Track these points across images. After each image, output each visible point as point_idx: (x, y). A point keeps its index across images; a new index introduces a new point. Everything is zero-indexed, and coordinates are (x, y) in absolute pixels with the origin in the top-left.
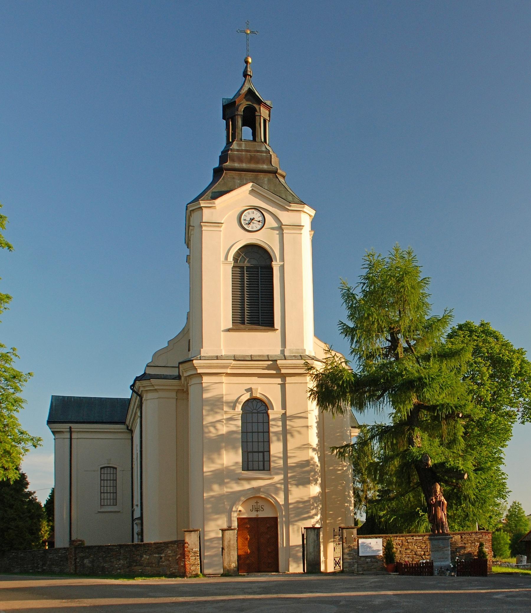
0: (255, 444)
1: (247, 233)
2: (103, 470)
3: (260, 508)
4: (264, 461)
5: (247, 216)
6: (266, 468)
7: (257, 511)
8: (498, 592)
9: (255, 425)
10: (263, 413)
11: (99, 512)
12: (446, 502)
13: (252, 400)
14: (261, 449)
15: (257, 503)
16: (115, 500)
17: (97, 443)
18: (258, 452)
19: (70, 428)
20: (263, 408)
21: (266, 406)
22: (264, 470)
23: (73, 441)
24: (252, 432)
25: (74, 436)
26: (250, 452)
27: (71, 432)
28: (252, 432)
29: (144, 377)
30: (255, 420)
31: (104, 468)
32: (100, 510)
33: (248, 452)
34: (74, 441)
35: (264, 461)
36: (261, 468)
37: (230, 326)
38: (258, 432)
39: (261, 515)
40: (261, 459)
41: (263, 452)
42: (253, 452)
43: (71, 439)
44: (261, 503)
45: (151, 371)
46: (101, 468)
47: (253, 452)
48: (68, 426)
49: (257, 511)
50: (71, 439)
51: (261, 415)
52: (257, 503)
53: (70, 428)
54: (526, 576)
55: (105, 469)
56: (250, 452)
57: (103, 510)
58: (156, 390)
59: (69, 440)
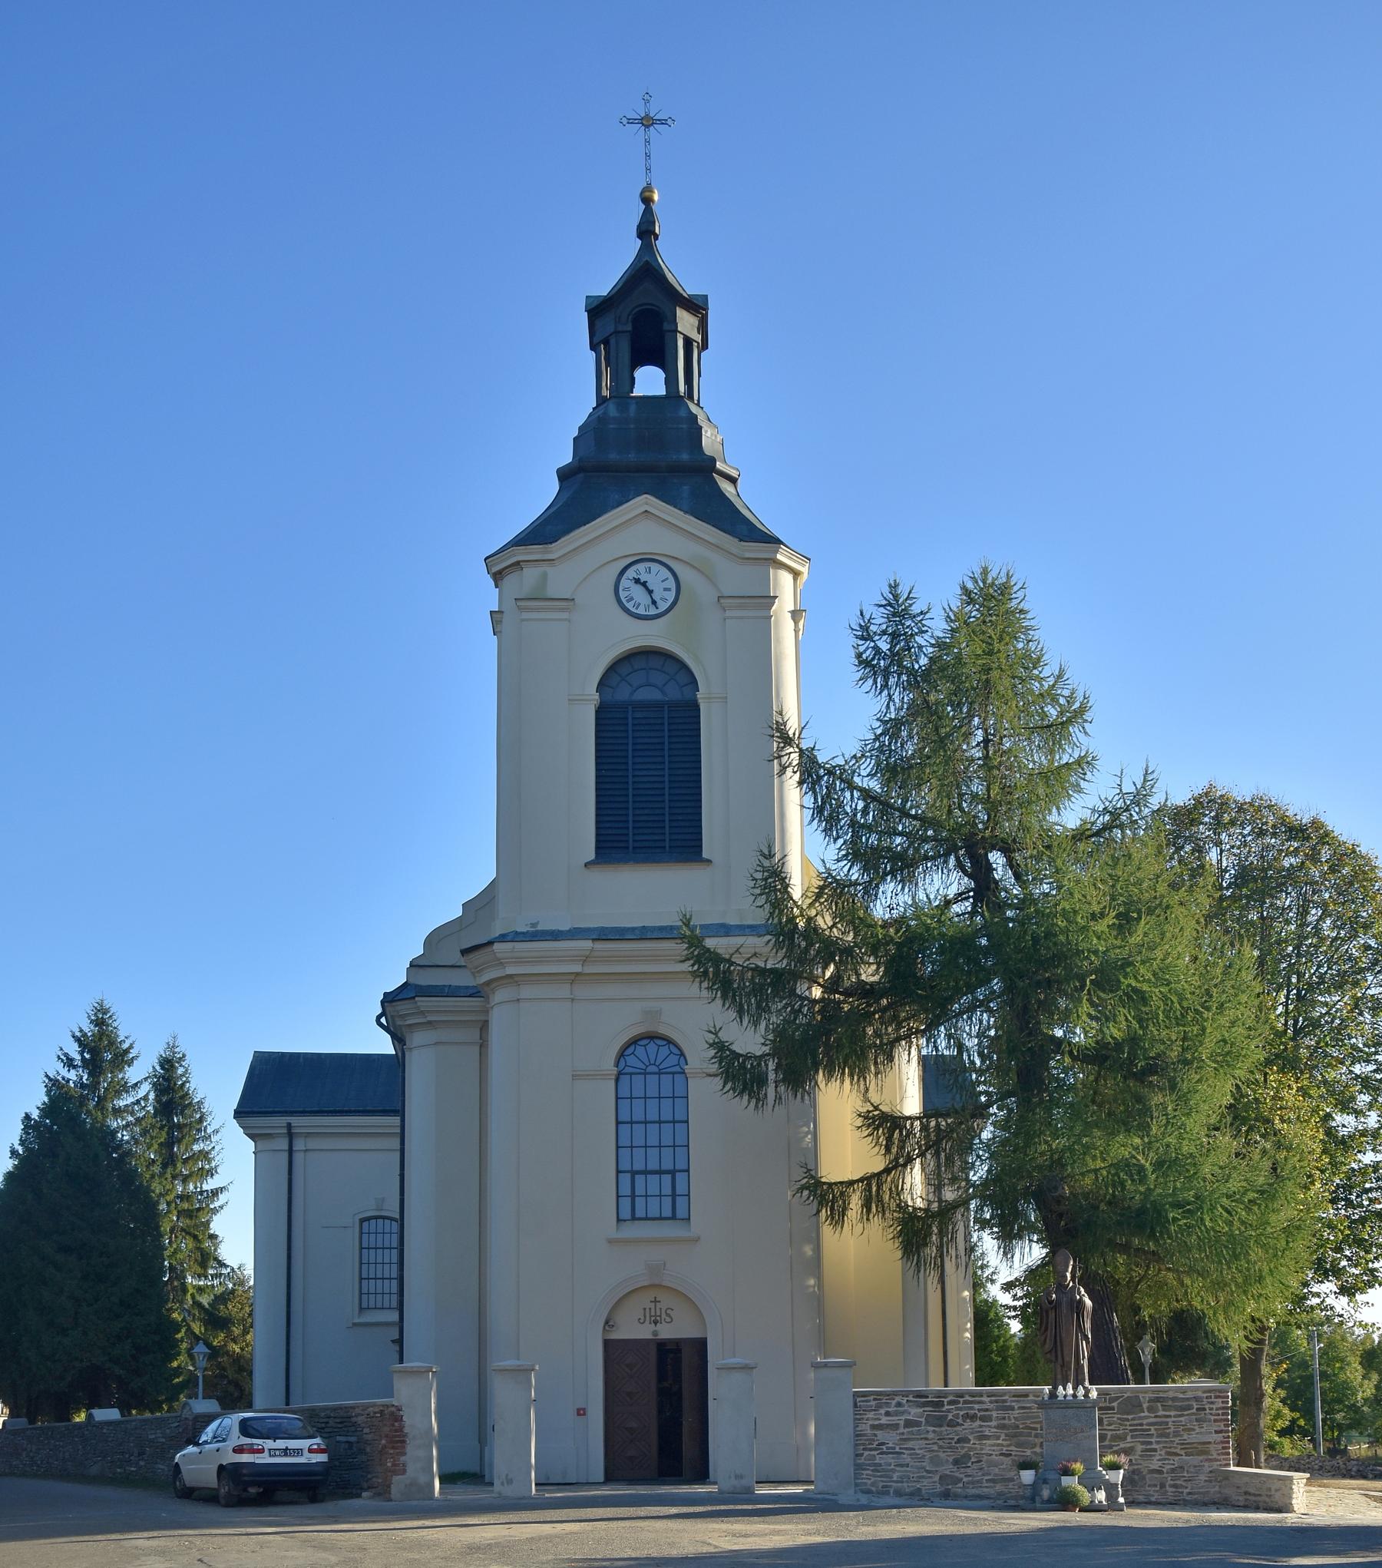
1: (616, 605)
2: (366, 1224)
3: (664, 1316)
4: (674, 1195)
5: (657, 577)
6: (680, 1213)
7: (656, 1323)
9: (653, 1153)
10: (673, 1073)
11: (355, 1324)
12: (1088, 1302)
13: (632, 1048)
14: (667, 1165)
15: (655, 1301)
16: (365, 1290)
17: (348, 1162)
18: (660, 1172)
19: (289, 1126)
21: (682, 1054)
22: (674, 1217)
24: (646, 1123)
25: (299, 1145)
27: (291, 1135)
28: (632, 1123)
30: (652, 1092)
31: (368, 1219)
32: (357, 1321)
33: (634, 1173)
34: (298, 1158)
35: (674, 1195)
37: (592, 856)
38: (660, 1122)
39: (666, 1332)
40: (667, 1190)
41: (673, 1173)
42: (646, 1172)
43: (291, 1151)
44: (666, 1301)
45: (426, 979)
46: (362, 1221)
47: (646, 1172)
48: (283, 1120)
49: (656, 1323)
50: (291, 1151)
51: (666, 1079)
52: (655, 1301)
53: (289, 1126)
54: (1012, 1502)
55: (373, 1221)
57: (361, 1320)
58: (430, 1022)
59: (286, 1155)
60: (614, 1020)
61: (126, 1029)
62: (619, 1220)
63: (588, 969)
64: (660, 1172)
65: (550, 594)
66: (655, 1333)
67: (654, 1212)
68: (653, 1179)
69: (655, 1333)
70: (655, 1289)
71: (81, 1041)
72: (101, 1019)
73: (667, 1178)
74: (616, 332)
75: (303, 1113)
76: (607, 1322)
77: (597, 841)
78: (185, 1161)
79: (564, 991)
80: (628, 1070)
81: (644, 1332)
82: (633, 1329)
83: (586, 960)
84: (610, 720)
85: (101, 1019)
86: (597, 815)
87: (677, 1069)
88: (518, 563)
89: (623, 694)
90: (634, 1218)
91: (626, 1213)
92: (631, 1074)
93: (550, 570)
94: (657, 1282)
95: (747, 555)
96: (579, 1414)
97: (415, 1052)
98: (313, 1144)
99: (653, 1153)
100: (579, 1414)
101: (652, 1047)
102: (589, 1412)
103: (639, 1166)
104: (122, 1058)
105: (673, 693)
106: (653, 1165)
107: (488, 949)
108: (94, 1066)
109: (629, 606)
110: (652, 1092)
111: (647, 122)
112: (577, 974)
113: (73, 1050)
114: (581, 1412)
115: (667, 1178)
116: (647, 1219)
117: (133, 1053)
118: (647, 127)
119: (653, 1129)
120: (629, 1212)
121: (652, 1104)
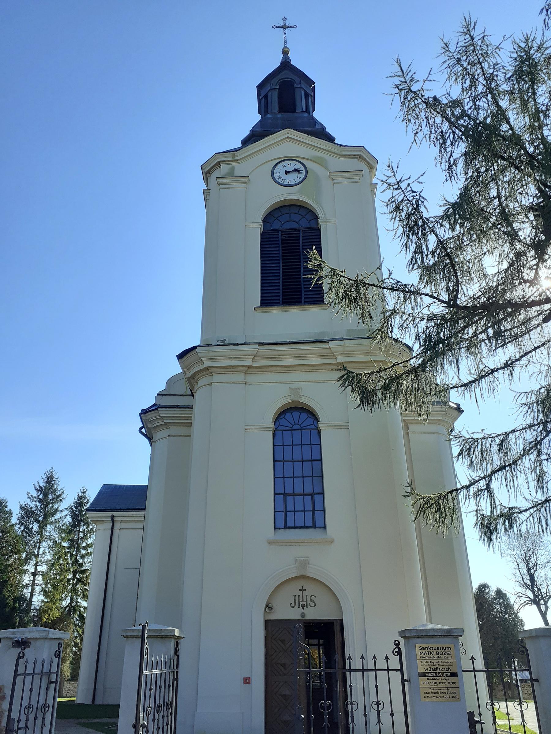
0: (298, 473)
3: (309, 601)
6: (319, 523)
7: (303, 606)
8: (310, 693)
9: (298, 481)
10: (310, 430)
14: (308, 490)
15: (303, 590)
18: (304, 494)
20: (310, 420)
22: (314, 527)
23: (114, 532)
25: (117, 526)
26: (290, 495)
27: (113, 521)
29: (155, 408)
30: (297, 441)
33: (286, 495)
34: (116, 533)
36: (309, 523)
38: (303, 461)
40: (309, 507)
41: (312, 495)
42: (294, 495)
47: (294, 495)
48: (110, 514)
49: (303, 606)
51: (306, 433)
52: (303, 590)
53: (113, 516)
56: (290, 495)
58: (166, 424)
59: (110, 530)
60: (270, 396)
61: (61, 485)
62: (275, 528)
63: (255, 364)
64: (304, 494)
65: (236, 175)
66: (303, 615)
67: (300, 523)
68: (299, 499)
69: (303, 615)
70: (302, 581)
71: (40, 490)
72: (50, 479)
73: (308, 499)
74: (271, 89)
75: (120, 510)
76: (267, 606)
77: (261, 241)
78: (84, 548)
79: (240, 377)
80: (280, 428)
81: (294, 614)
82: (286, 612)
83: (254, 358)
84: (267, 238)
85: (50, 479)
86: (262, 280)
87: (313, 427)
88: (219, 162)
89: (276, 225)
90: (286, 527)
91: (281, 524)
92: (283, 430)
93: (236, 166)
94: (304, 574)
95: (344, 153)
96: (245, 683)
97: (157, 443)
98: (124, 525)
99: (298, 481)
100: (245, 683)
101: (296, 414)
102: (253, 681)
103: (289, 490)
104: (58, 498)
105: (304, 224)
106: (299, 490)
107: (194, 352)
108: (44, 502)
109: (280, 181)
110: (297, 441)
111: (285, 27)
112: (249, 367)
113: (34, 493)
114: (247, 681)
115: (308, 499)
116: (295, 527)
117: (64, 495)
118: (285, 28)
119: (297, 456)
120: (284, 520)
121: (297, 449)
